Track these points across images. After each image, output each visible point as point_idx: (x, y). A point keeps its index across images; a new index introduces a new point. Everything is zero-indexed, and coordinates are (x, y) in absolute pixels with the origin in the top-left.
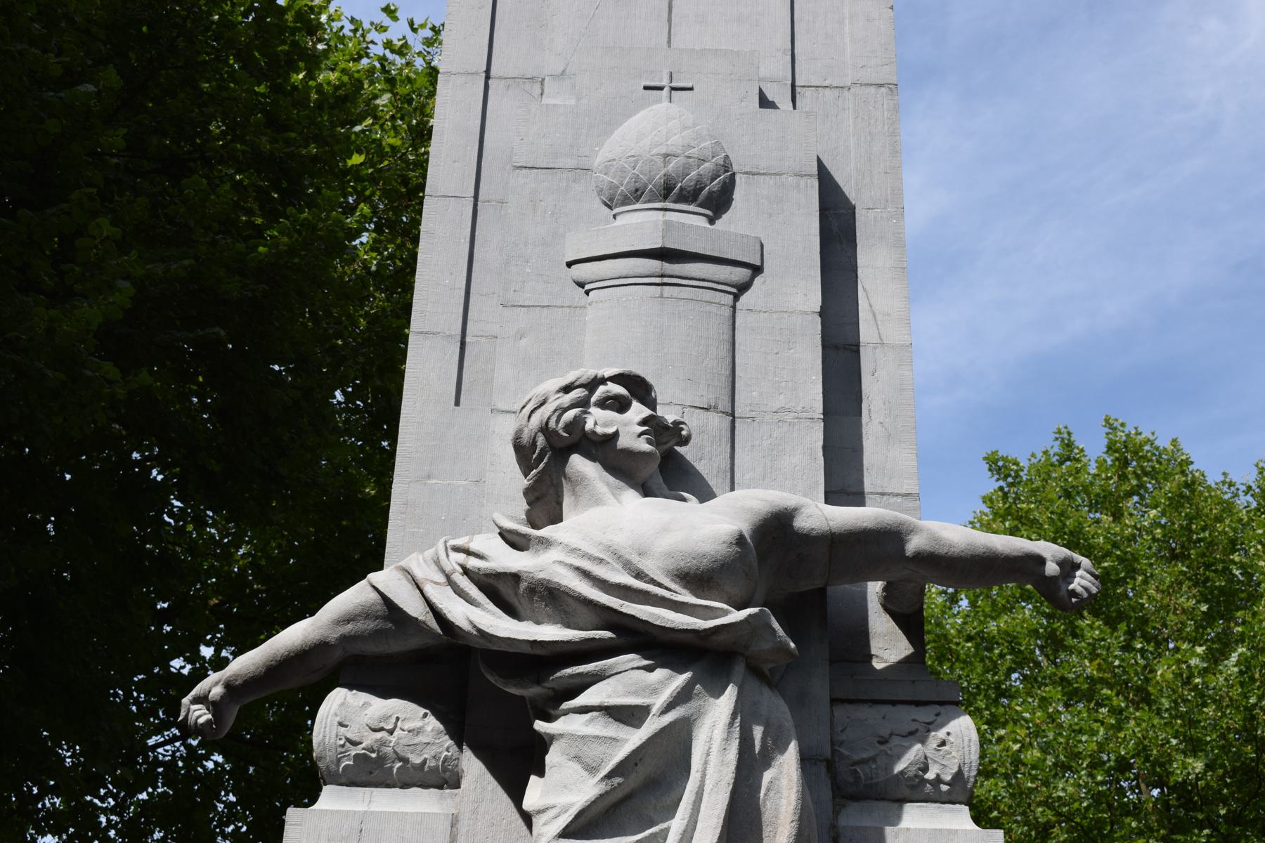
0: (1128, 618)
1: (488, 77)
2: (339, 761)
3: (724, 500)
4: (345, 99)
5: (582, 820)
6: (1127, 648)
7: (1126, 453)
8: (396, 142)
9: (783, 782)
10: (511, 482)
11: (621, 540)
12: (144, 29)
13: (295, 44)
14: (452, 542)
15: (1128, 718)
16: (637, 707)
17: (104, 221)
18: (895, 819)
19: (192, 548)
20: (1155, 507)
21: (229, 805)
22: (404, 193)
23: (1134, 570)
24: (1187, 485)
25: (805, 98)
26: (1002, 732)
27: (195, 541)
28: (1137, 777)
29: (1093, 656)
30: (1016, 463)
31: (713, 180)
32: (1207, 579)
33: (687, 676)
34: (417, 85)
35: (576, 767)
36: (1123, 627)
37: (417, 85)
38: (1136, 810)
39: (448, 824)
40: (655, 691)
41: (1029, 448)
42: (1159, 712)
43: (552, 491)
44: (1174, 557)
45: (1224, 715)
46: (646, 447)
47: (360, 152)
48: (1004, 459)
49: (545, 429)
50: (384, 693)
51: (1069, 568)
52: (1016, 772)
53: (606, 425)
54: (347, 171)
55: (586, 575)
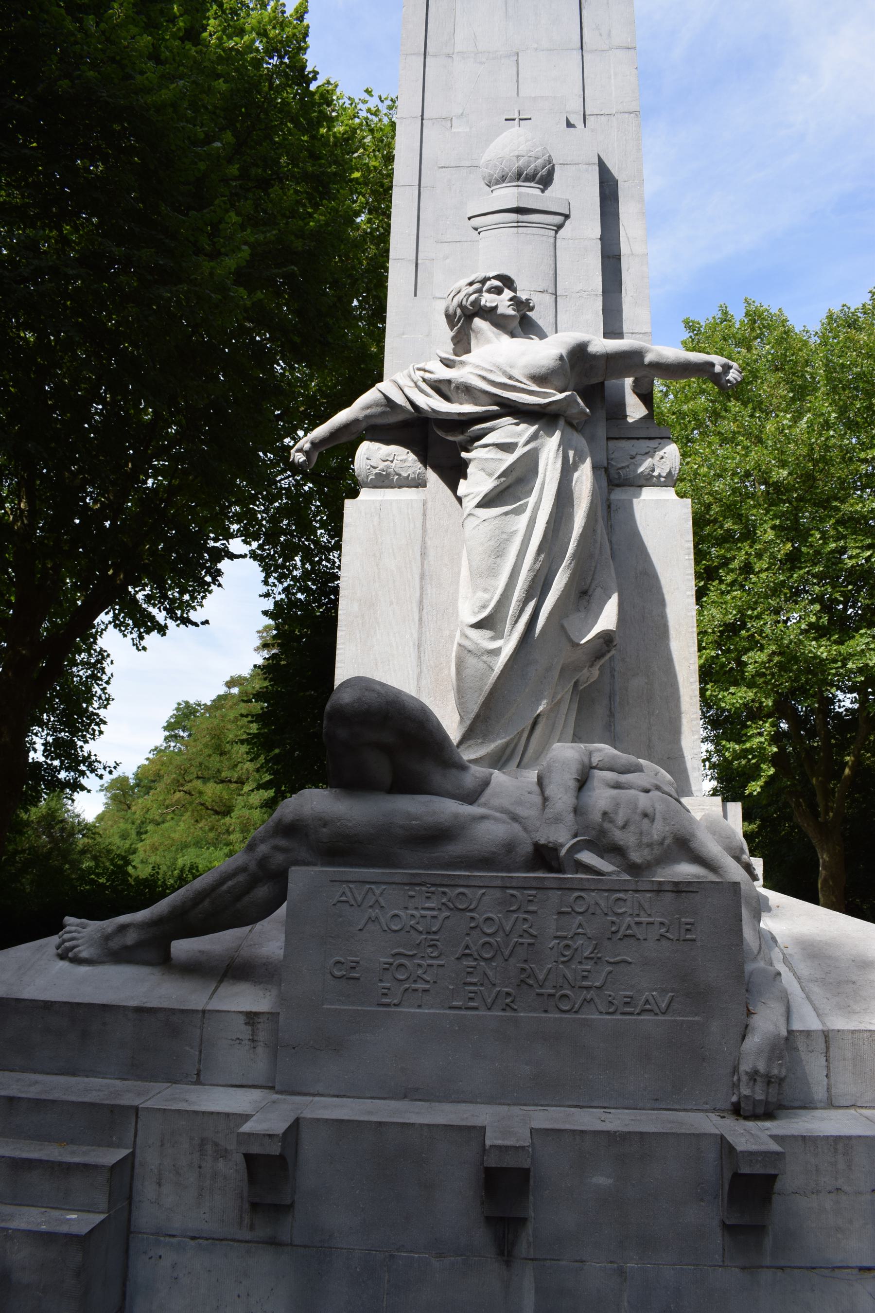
0: (753, 401)
1: (422, 119)
2: (368, 476)
3: (552, 339)
4: (348, 139)
5: (486, 499)
6: (752, 416)
7: (755, 317)
8: (376, 164)
9: (584, 479)
10: (446, 333)
11: (501, 360)
12: (243, 110)
13: (320, 112)
14: (416, 366)
15: (751, 451)
16: (511, 443)
17: (232, 214)
18: (638, 495)
19: (289, 383)
20: (769, 344)
21: (317, 507)
22: (382, 192)
23: (757, 377)
24: (785, 333)
25: (590, 121)
26: (689, 460)
27: (290, 380)
28: (754, 480)
29: (735, 420)
30: (699, 324)
31: (543, 169)
32: (793, 381)
33: (536, 427)
34: (385, 132)
35: (483, 474)
36: (750, 405)
37: (385, 132)
38: (753, 496)
39: (422, 504)
40: (520, 435)
41: (705, 316)
42: (766, 448)
43: (465, 337)
44: (777, 369)
45: (798, 448)
46: (513, 313)
47: (358, 171)
48: (692, 321)
49: (460, 305)
50: (387, 442)
51: (727, 368)
52: (695, 479)
53: (491, 302)
54: (351, 180)
55: (484, 378)
